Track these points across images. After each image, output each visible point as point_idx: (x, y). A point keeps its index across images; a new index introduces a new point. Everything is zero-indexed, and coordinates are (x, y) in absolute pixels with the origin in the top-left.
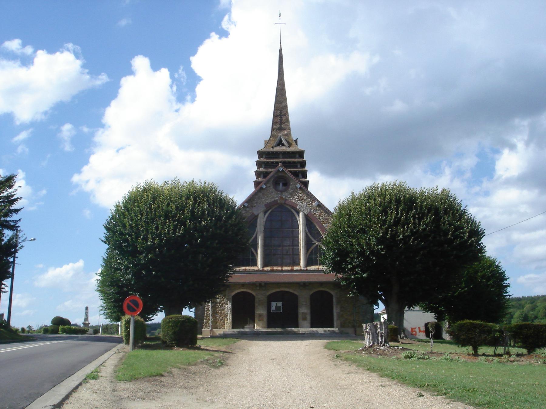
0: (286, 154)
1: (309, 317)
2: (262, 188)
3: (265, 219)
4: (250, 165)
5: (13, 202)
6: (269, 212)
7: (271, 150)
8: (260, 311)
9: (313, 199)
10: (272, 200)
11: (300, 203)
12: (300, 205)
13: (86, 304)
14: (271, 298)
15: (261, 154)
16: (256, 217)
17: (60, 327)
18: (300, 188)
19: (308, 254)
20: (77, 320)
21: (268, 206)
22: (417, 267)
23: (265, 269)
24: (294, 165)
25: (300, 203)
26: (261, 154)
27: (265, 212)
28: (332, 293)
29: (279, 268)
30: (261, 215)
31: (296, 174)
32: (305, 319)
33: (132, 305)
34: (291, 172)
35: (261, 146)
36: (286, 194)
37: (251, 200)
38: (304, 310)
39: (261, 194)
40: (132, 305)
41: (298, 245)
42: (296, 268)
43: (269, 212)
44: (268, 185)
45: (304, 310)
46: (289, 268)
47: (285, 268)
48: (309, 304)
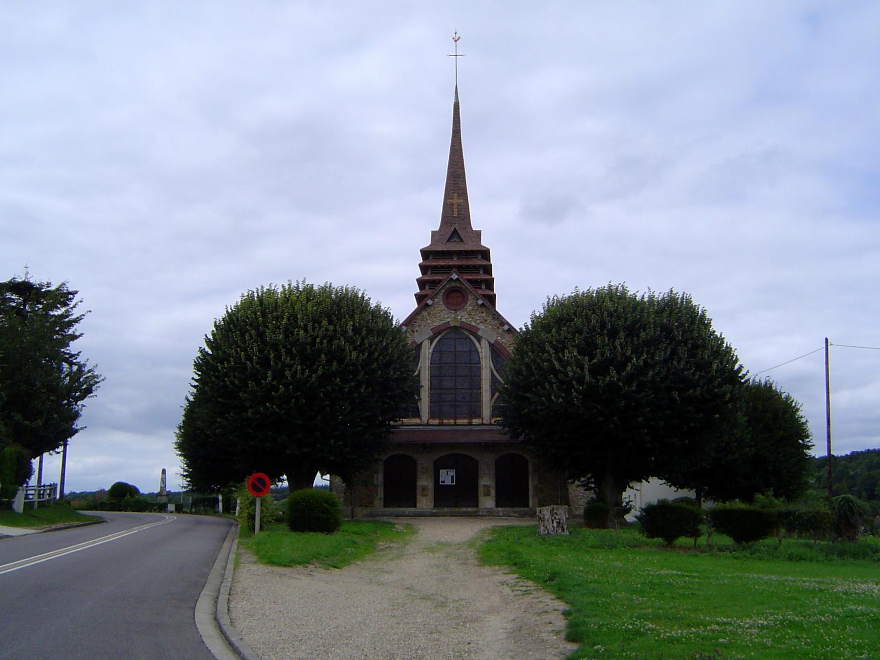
0: (460, 254)
1: (493, 492)
2: (427, 305)
3: (431, 351)
4: (411, 271)
5: (70, 324)
6: (438, 339)
7: (440, 248)
8: (425, 482)
9: (502, 322)
10: (442, 322)
11: (482, 326)
12: (484, 329)
13: (158, 463)
14: (439, 465)
15: (425, 253)
16: (419, 347)
17: (123, 498)
18: (483, 305)
19: (493, 401)
20: (148, 486)
21: (437, 332)
22: (632, 415)
23: (432, 422)
24: (475, 269)
25: (482, 326)
26: (425, 253)
27: (432, 340)
28: (528, 457)
29: (452, 421)
30: (426, 343)
31: (476, 284)
32: (487, 494)
33: (258, 484)
34: (469, 281)
35: (426, 242)
36: (463, 313)
37: (411, 320)
38: (486, 481)
39: (425, 313)
40: (258, 484)
41: (479, 388)
42: (475, 421)
43: (438, 339)
44: (436, 300)
45: (486, 481)
46: (466, 421)
47: (459, 421)
48: (493, 472)
